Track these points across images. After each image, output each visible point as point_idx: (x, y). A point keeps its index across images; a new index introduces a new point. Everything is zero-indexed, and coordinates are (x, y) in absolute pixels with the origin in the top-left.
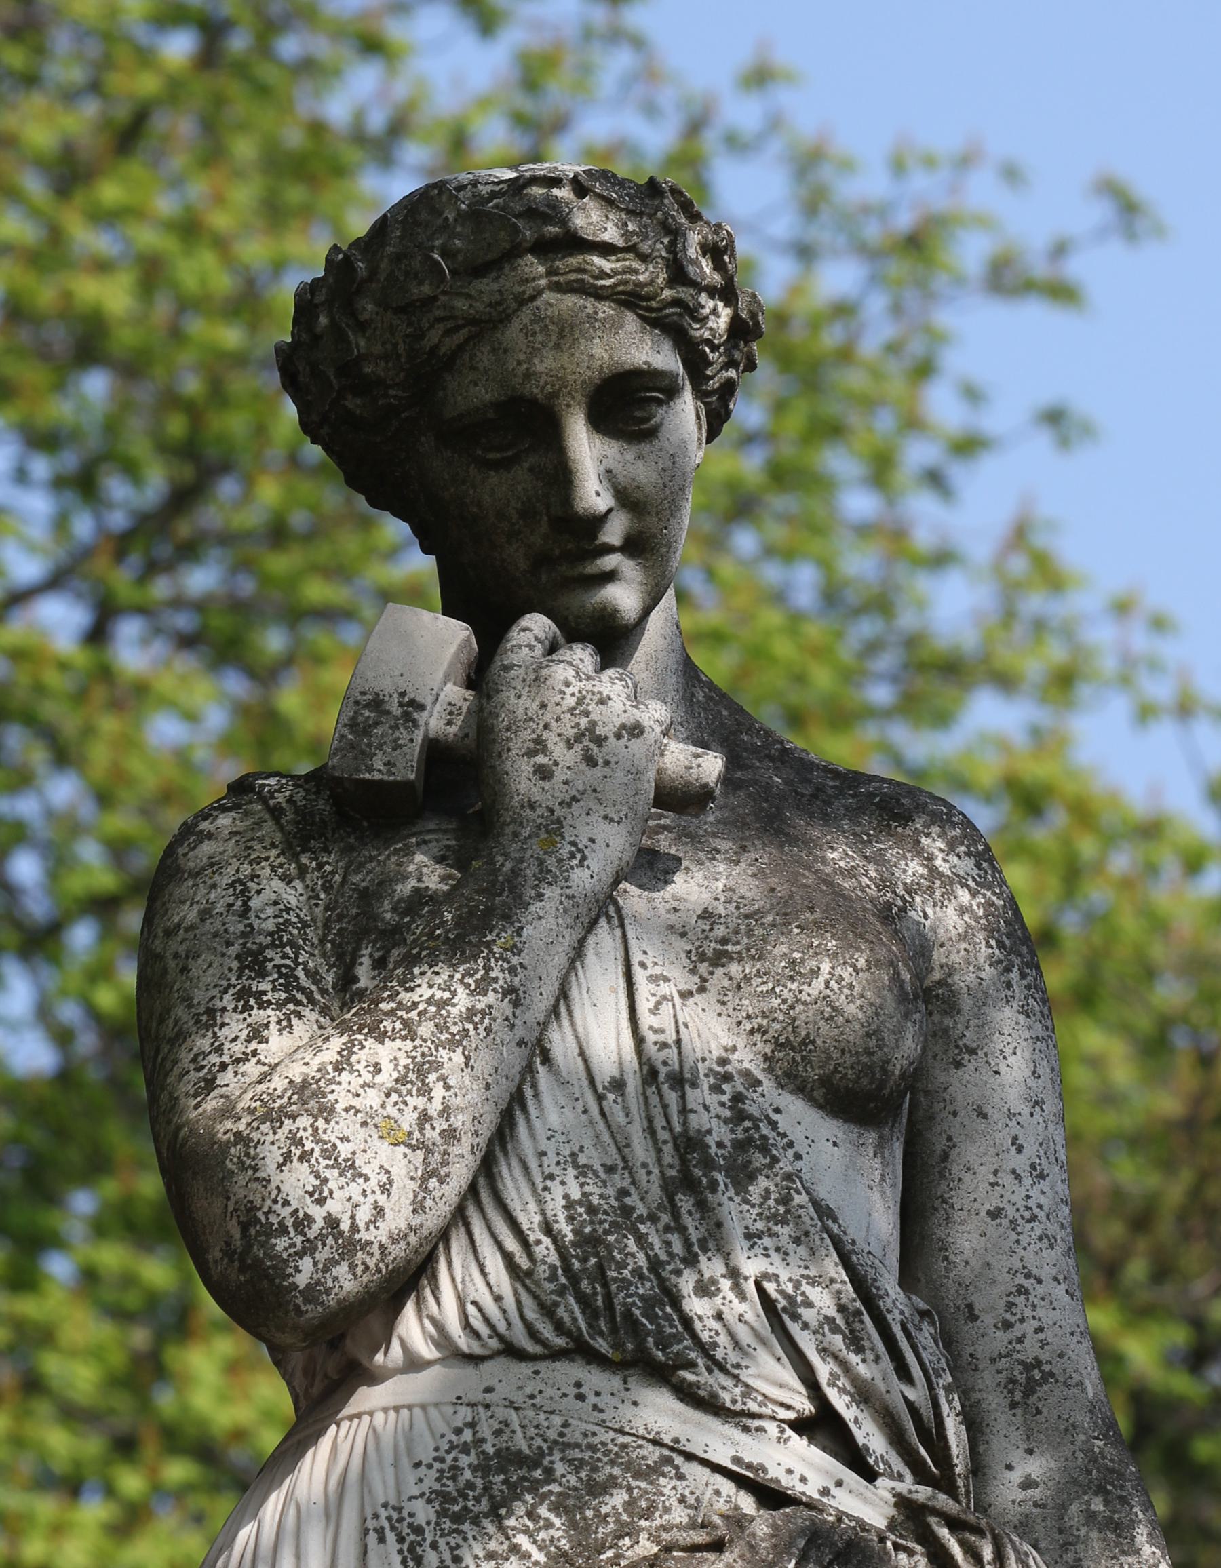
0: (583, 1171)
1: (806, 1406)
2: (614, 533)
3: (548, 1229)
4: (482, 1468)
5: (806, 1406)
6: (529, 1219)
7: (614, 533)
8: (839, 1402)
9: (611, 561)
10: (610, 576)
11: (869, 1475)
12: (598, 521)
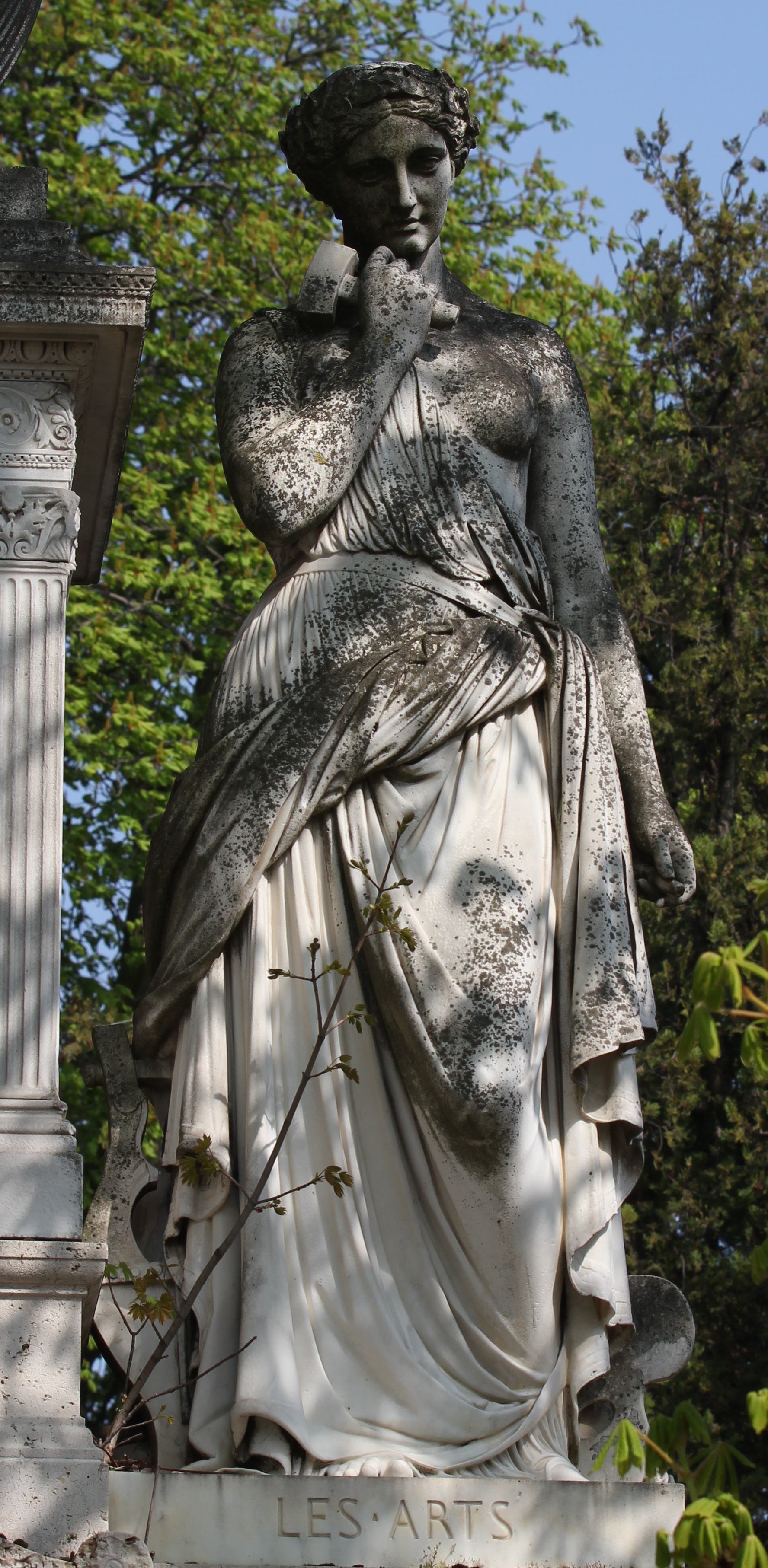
0: (398, 476)
1: (486, 575)
2: (416, 214)
3: (383, 500)
4: (354, 598)
5: (486, 575)
6: (375, 496)
7: (416, 214)
8: (500, 574)
9: (414, 226)
10: (414, 232)
11: (512, 604)
12: (410, 209)
